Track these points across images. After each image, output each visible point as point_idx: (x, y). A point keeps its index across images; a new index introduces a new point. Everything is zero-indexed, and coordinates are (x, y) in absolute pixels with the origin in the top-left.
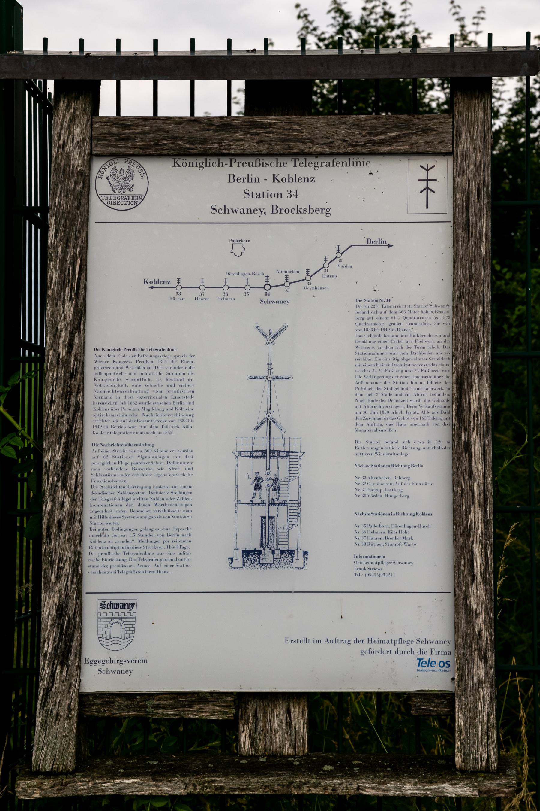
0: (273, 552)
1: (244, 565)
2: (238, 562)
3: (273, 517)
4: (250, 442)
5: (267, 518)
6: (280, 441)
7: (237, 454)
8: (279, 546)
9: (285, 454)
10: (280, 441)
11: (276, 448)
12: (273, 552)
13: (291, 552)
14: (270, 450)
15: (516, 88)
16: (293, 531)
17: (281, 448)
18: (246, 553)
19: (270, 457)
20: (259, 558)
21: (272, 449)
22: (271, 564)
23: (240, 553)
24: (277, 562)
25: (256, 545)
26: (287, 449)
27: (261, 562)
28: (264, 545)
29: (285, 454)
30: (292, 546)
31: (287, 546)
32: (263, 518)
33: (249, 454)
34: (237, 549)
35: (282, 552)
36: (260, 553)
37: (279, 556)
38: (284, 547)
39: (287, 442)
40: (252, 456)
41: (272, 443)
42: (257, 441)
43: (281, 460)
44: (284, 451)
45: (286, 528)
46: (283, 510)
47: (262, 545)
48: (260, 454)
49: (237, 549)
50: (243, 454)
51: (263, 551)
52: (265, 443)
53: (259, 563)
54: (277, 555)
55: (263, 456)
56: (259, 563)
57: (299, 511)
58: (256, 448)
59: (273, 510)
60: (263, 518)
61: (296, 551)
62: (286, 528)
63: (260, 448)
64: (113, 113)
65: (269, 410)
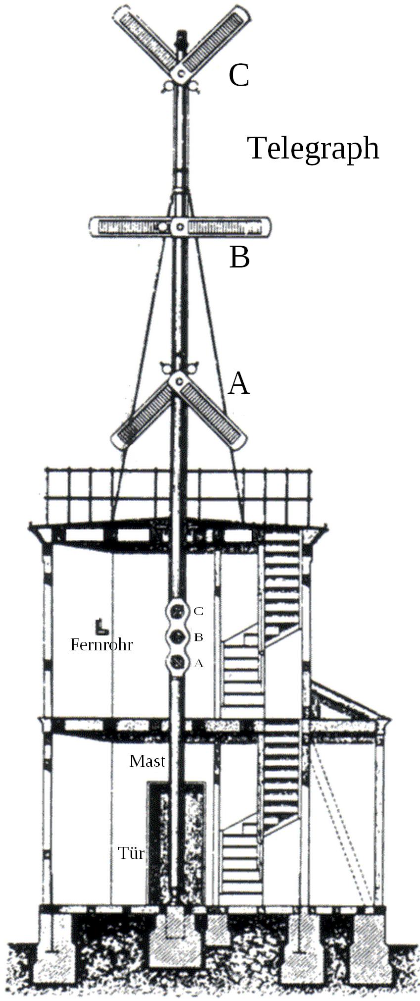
0: (201, 925)
1: (81, 974)
2: (55, 965)
3: (198, 789)
4: (102, 485)
5: (175, 787)
6: (225, 485)
7: (47, 535)
8: (225, 900)
9: (245, 536)
10: (225, 485)
11: (211, 512)
12: (201, 925)
13: (274, 925)
14: (185, 521)
15: (148, 782)
16: (281, 844)
17: (229, 512)
18: (91, 927)
19: (185, 549)
20: (144, 946)
21: (192, 511)
22: (192, 971)
23: (64, 926)
24: (214, 966)
25: (130, 890)
26: (254, 514)
27: (154, 962)
28: (166, 896)
29: (245, 536)
30: (278, 896)
31: (257, 900)
32: (157, 790)
33: (98, 535)
34: (51, 909)
35: (238, 924)
36: (146, 924)
37: (225, 939)
38: (244, 905)
39: (254, 486)
40: (111, 545)
41: (192, 492)
42: (132, 485)
43: (230, 560)
44: (242, 525)
45: (252, 830)
46: (241, 759)
47: (154, 896)
48: (143, 535)
49: (51, 909)
50: (72, 535)
51: (160, 919)
52: (164, 491)
53: (145, 965)
54: (218, 934)
55: (155, 546)
56: (145, 965)
57: (303, 763)
58: (125, 512)
59: (199, 760)
60: (157, 790)
61: (293, 919)
62: (252, 830)
63: (144, 511)
64: (196, 516)
65: (180, 358)
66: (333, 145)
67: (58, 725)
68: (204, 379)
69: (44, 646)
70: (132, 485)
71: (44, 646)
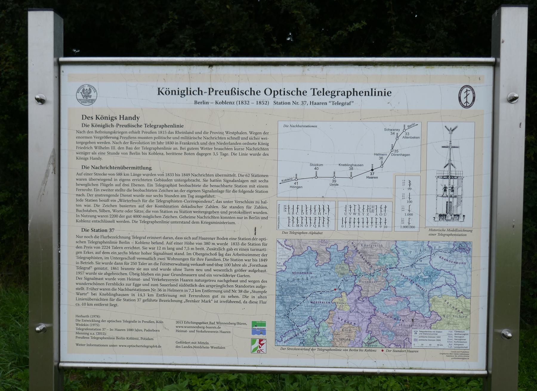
2: (437, 219)
11: (453, 175)
13: (458, 215)
16: (459, 208)
18: (440, 215)
30: (459, 213)
32: (447, 202)
35: (455, 215)
36: (446, 215)
40: (443, 178)
42: (445, 172)
46: (455, 199)
54: (453, 216)
55: (447, 178)
59: (451, 200)
60: (447, 202)
66: (219, 302)
67: (438, 196)
68: (452, 162)
69: (251, 155)
70: (445, 172)
71: (251, 155)
